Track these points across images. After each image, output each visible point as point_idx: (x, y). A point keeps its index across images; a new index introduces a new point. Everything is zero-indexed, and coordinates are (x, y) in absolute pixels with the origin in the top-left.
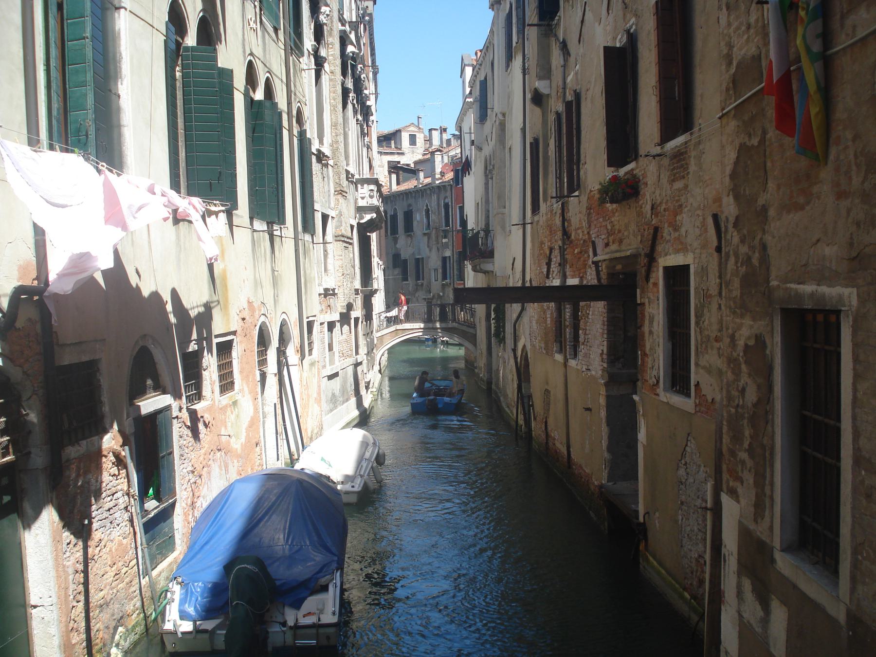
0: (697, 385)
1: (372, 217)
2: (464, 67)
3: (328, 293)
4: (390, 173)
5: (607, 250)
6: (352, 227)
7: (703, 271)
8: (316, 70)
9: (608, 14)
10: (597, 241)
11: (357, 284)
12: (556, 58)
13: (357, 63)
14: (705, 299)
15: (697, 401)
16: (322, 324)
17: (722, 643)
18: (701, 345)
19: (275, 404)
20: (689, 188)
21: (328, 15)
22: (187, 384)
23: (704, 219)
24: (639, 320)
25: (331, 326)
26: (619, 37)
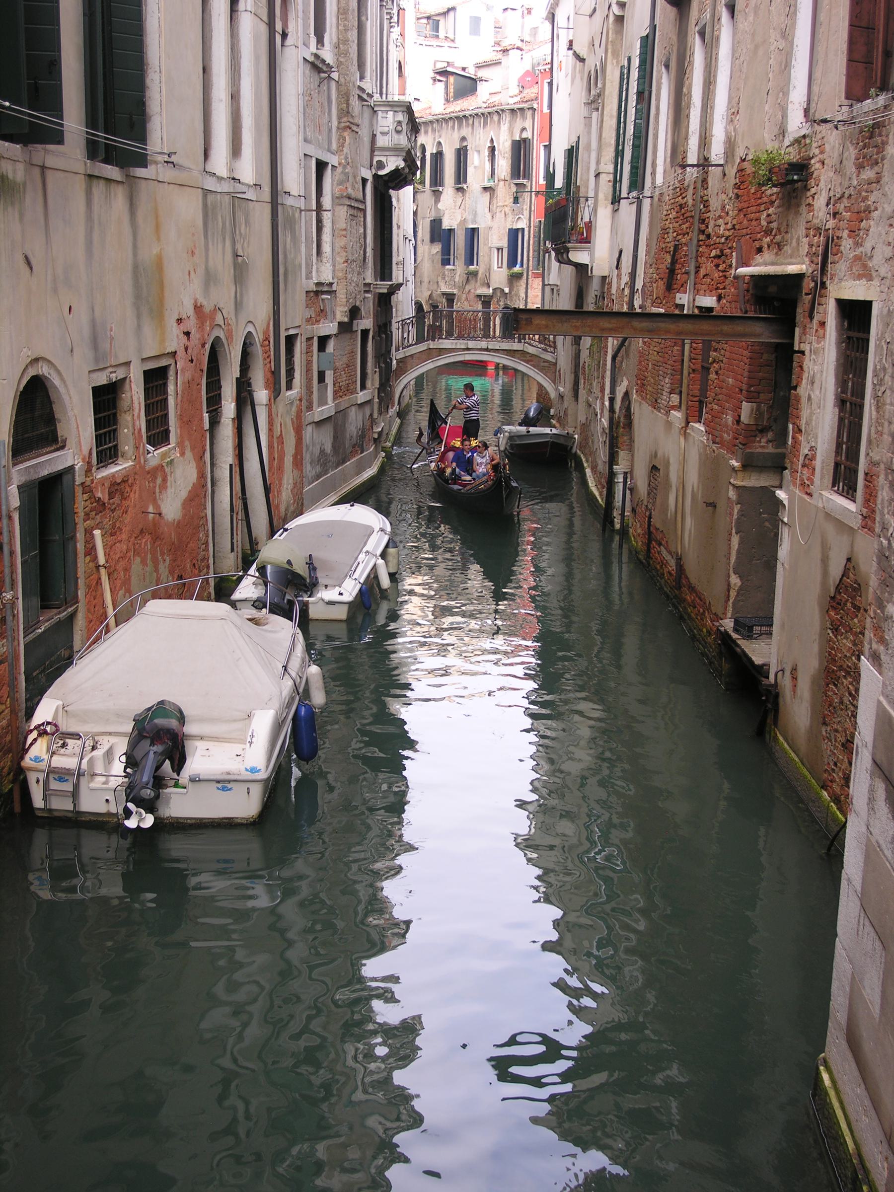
3: (320, 291)
16: (309, 339)
19: (231, 465)
22: (101, 432)
25: (323, 341)
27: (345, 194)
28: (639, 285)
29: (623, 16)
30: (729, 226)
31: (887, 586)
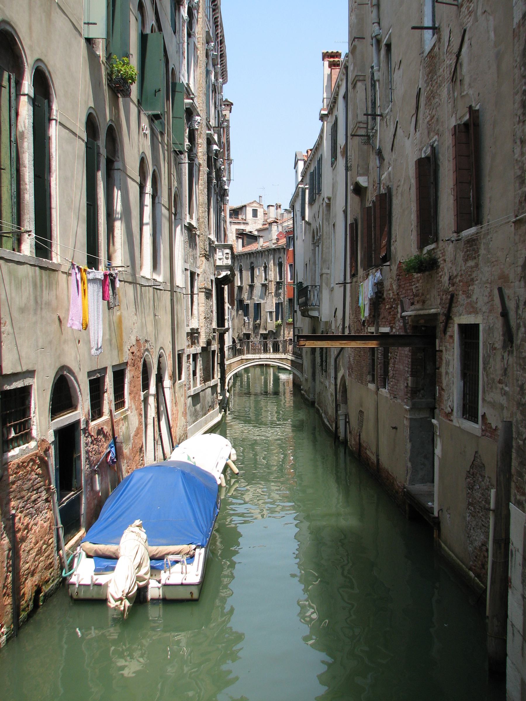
0: (484, 416)
1: (227, 273)
2: (297, 161)
4: (237, 238)
5: (413, 307)
6: (212, 281)
7: (490, 330)
8: (189, 163)
9: (416, 131)
10: (404, 300)
11: (214, 325)
12: (374, 161)
13: (219, 158)
14: (491, 351)
15: (483, 427)
17: (509, 617)
18: (487, 385)
19: (154, 418)
20: (479, 266)
21: (199, 123)
23: (491, 291)
24: (437, 363)
25: (195, 356)
26: (424, 149)
27: (204, 287)
28: (347, 324)
29: (330, 204)
30: (395, 293)
31: (524, 465)
